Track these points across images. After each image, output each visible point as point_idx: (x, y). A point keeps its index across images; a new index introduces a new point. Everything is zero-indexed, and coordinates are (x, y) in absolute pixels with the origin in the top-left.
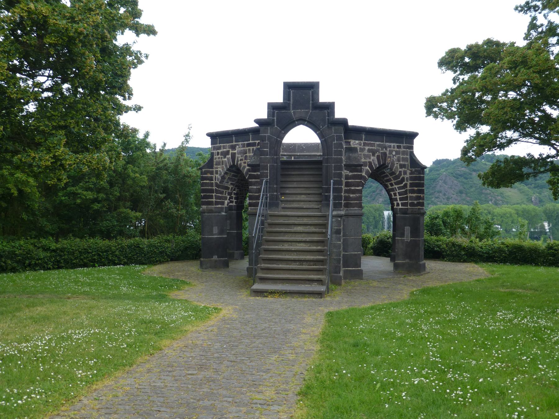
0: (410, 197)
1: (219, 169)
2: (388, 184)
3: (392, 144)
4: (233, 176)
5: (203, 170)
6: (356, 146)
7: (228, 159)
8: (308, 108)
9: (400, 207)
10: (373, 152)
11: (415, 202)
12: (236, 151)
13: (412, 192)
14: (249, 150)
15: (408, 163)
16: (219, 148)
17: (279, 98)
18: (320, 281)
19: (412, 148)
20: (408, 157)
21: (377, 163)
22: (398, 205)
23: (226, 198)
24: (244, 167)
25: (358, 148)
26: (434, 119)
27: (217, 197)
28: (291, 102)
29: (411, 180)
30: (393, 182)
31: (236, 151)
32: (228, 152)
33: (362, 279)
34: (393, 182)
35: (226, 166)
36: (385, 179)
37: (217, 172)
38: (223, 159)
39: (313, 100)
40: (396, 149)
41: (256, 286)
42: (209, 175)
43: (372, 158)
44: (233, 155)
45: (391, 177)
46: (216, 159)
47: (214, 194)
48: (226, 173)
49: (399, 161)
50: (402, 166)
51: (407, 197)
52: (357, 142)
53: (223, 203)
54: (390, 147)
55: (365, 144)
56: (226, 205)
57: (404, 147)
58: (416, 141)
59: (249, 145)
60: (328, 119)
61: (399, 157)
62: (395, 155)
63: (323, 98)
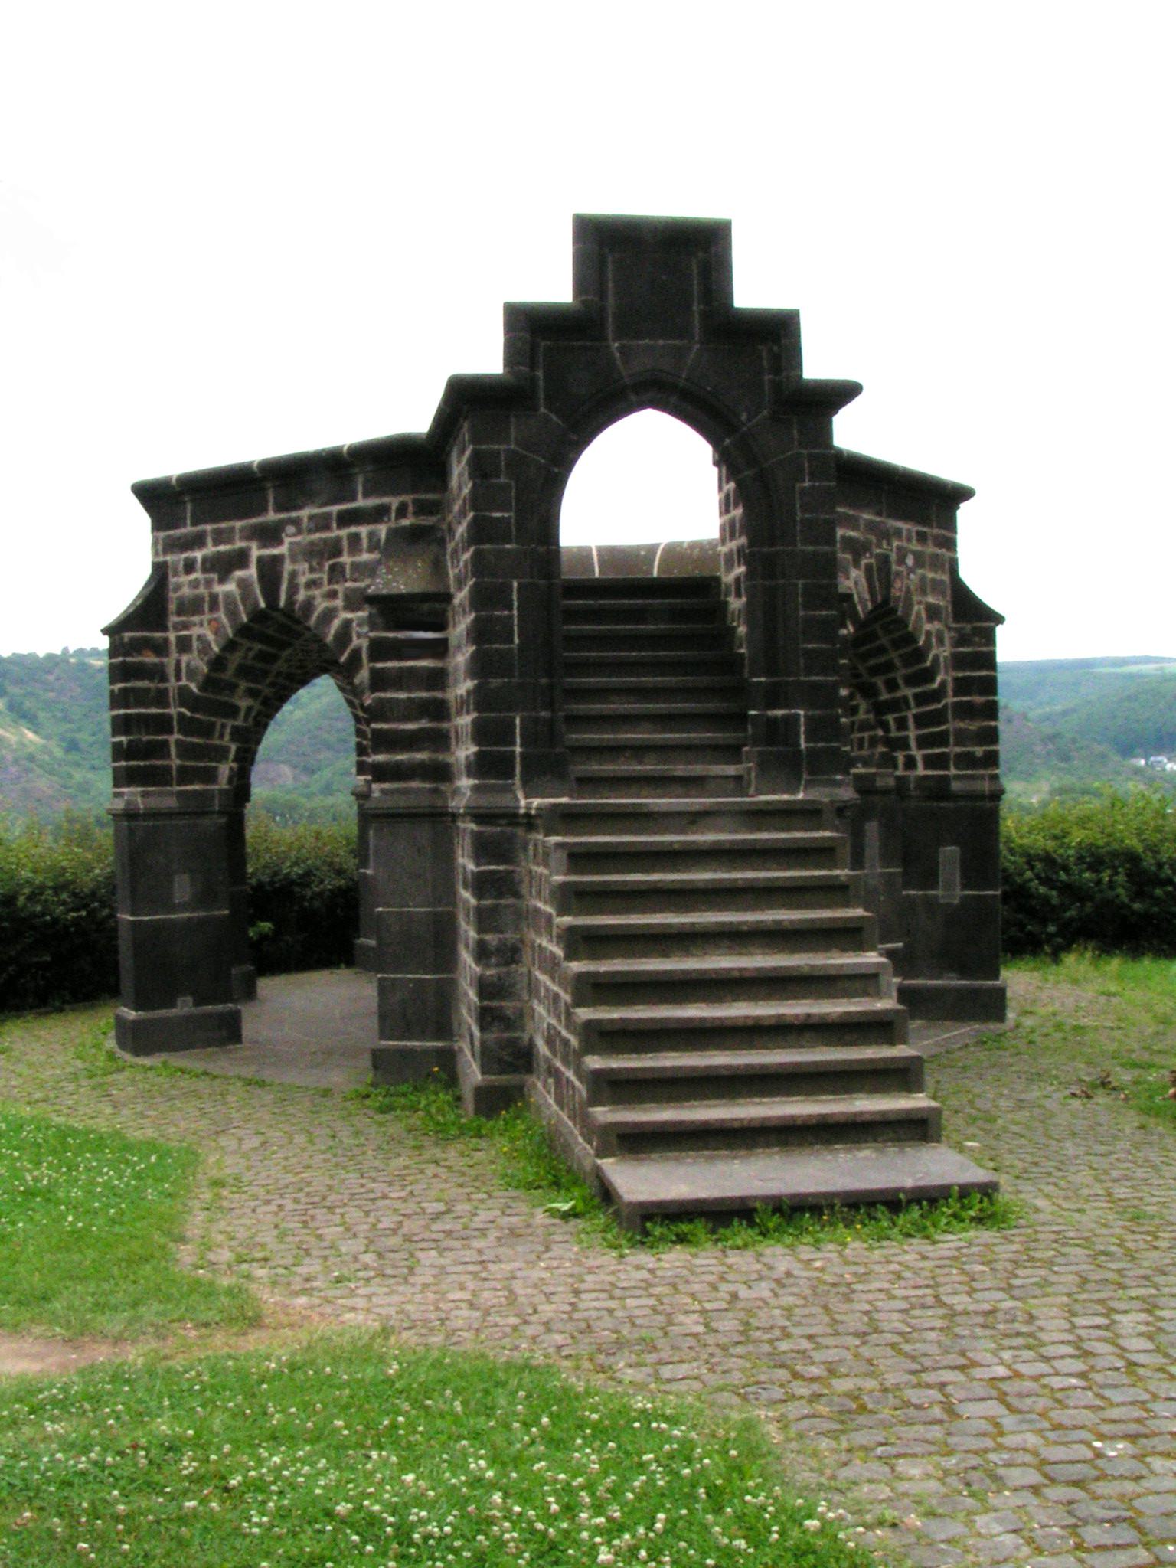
1: (195, 632)
2: (879, 681)
4: (262, 657)
5: (127, 635)
7: (243, 584)
8: (684, 332)
9: (921, 771)
12: (283, 550)
14: (355, 539)
15: (943, 602)
16: (198, 541)
17: (555, 286)
19: (950, 544)
20: (946, 578)
21: (867, 596)
23: (221, 754)
27: (185, 750)
28: (611, 302)
31: (283, 550)
34: (899, 674)
35: (232, 614)
37: (184, 645)
38: (220, 589)
40: (915, 546)
42: (150, 659)
44: (270, 570)
45: (894, 655)
48: (230, 646)
50: (933, 613)
53: (210, 776)
54: (898, 533)
58: (965, 513)
59: (346, 519)
63: (750, 292)
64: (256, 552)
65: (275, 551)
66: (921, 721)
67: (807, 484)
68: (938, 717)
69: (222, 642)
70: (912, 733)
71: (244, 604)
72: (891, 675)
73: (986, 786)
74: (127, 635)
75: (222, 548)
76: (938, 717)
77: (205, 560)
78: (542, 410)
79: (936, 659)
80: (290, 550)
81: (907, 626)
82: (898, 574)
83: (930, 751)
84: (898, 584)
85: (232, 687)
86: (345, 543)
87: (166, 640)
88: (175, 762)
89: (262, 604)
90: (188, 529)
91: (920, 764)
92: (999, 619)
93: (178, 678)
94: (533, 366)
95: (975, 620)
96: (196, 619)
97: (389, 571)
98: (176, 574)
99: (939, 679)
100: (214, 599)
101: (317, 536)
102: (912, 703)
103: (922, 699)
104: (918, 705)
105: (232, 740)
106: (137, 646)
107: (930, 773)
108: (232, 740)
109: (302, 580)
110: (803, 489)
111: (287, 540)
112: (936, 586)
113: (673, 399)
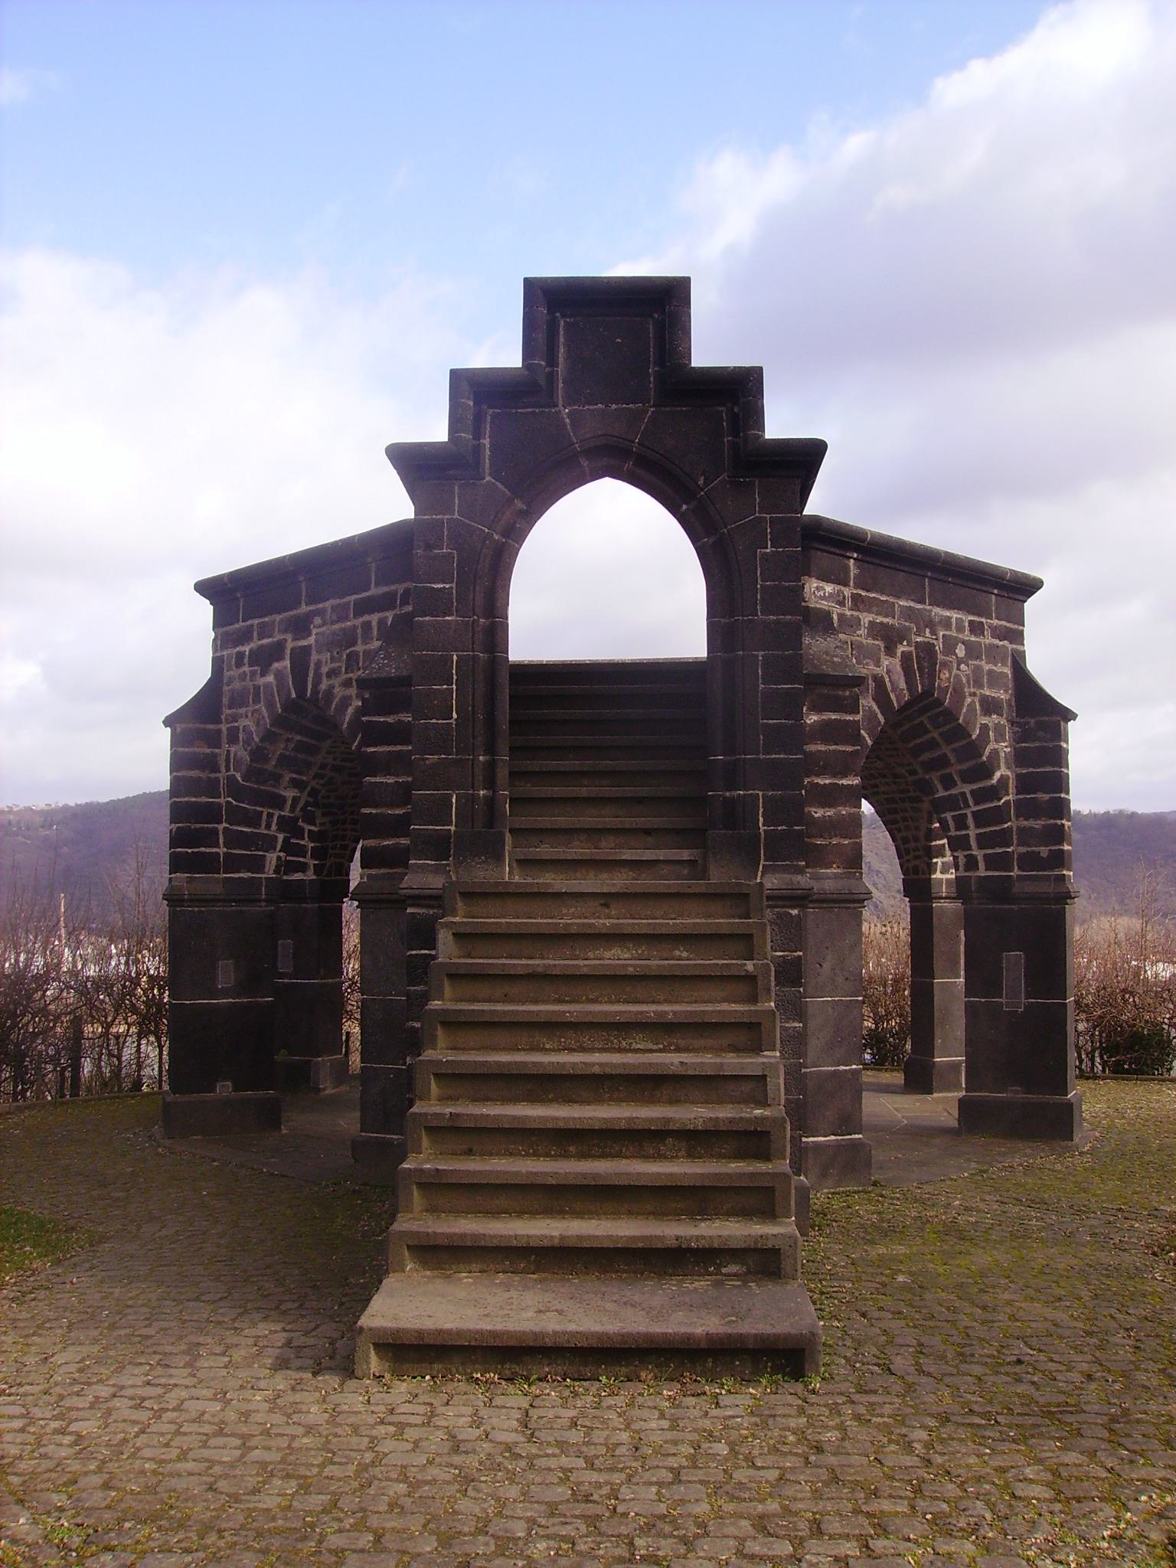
0: (1022, 830)
1: (242, 723)
2: (935, 777)
3: (954, 615)
4: (301, 747)
6: (824, 605)
7: (279, 675)
9: (982, 872)
12: (312, 640)
14: (367, 626)
16: (245, 637)
17: (502, 349)
19: (1017, 637)
20: (1008, 671)
21: (903, 685)
23: (269, 843)
24: (345, 702)
25: (835, 617)
27: (233, 839)
32: (280, 646)
34: (955, 769)
35: (270, 705)
36: (925, 757)
37: (233, 738)
38: (261, 681)
39: (661, 362)
40: (967, 636)
44: (301, 659)
45: (946, 749)
46: (231, 680)
47: (221, 827)
48: (269, 737)
50: (990, 706)
52: (829, 588)
53: (258, 864)
54: (946, 623)
55: (858, 602)
56: (269, 872)
59: (365, 607)
61: (978, 668)
63: (710, 347)
65: (304, 643)
66: (980, 819)
70: (972, 832)
72: (947, 771)
73: (1050, 888)
75: (265, 641)
78: (488, 478)
79: (995, 752)
82: (944, 664)
83: (990, 851)
84: (945, 675)
85: (277, 778)
87: (219, 731)
89: (294, 695)
91: (982, 865)
92: (1068, 715)
93: (228, 769)
94: (478, 435)
95: (1041, 719)
96: (242, 711)
99: (997, 775)
101: (336, 627)
103: (981, 796)
105: (280, 829)
107: (990, 873)
108: (280, 829)
111: (314, 631)
112: (994, 679)
113: (629, 464)
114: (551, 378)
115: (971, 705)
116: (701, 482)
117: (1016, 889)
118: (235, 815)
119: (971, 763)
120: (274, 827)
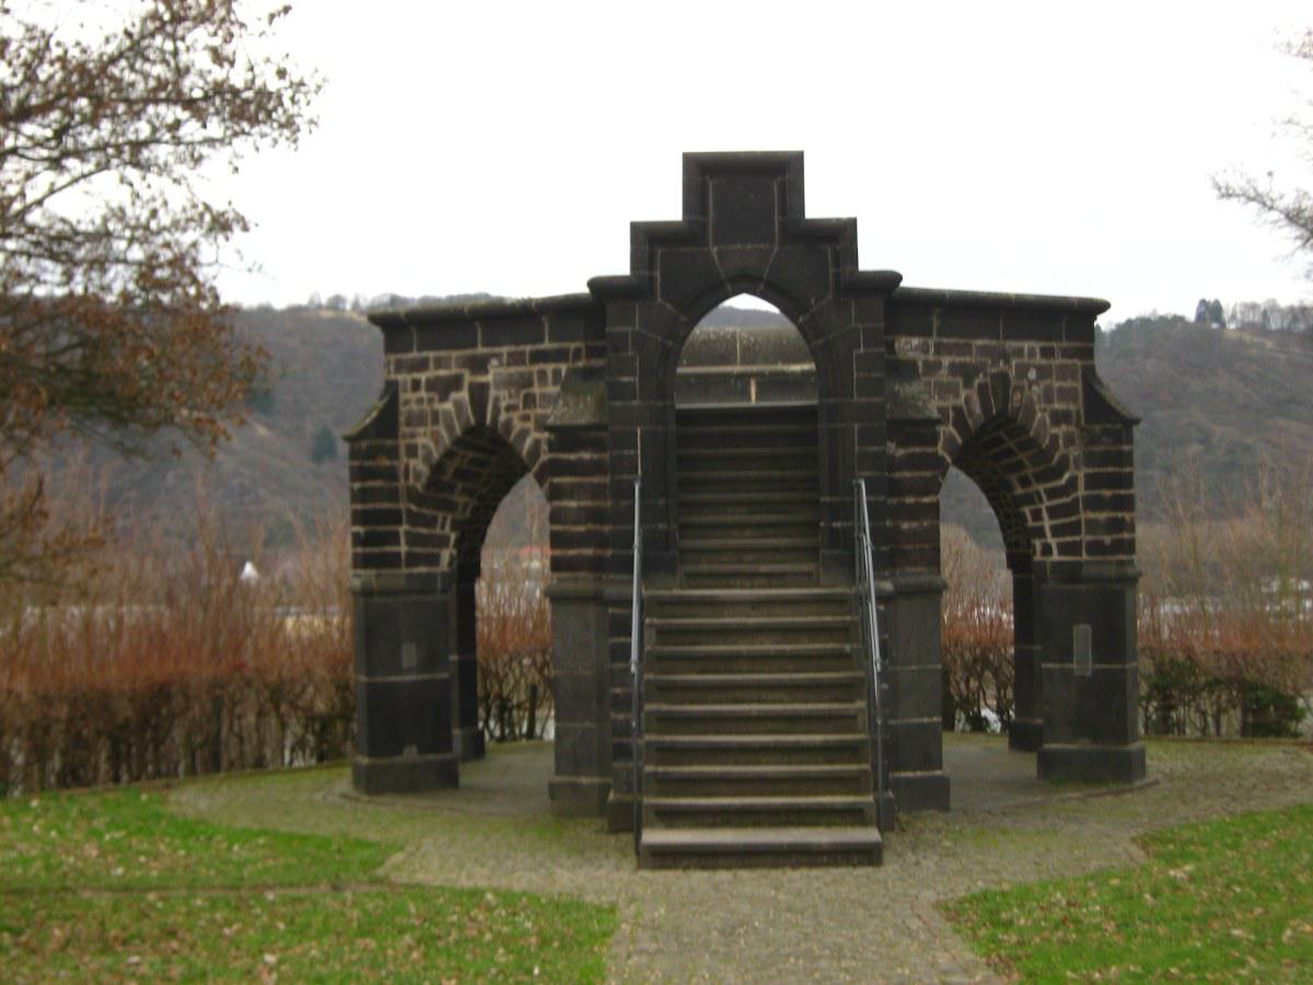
0: (1089, 522)
2: (1014, 478)
3: (1026, 345)
5: (364, 444)
6: (911, 355)
7: (458, 404)
9: (1056, 557)
10: (966, 373)
11: (1107, 539)
12: (489, 378)
13: (1095, 504)
14: (542, 374)
16: (422, 365)
17: (668, 207)
18: (853, 816)
20: (1079, 385)
21: (978, 410)
22: (1047, 550)
23: (443, 542)
25: (920, 363)
26: (1210, 298)
27: (413, 540)
29: (1087, 465)
30: (1029, 471)
31: (489, 378)
33: (946, 808)
34: (1029, 471)
35: (450, 428)
36: (1004, 462)
38: (438, 406)
39: (783, 212)
40: (1039, 360)
41: (654, 836)
42: (386, 462)
43: (963, 394)
44: (479, 394)
45: (1022, 456)
48: (449, 455)
49: (1048, 398)
50: (1059, 418)
51: (1079, 522)
52: (915, 341)
53: (434, 560)
54: (1019, 352)
55: (939, 349)
57: (1066, 353)
59: (538, 357)
60: (837, 276)
62: (1036, 382)
63: (819, 205)
64: (468, 378)
67: (862, 350)
68: (1072, 509)
69: (441, 450)
71: (459, 420)
74: (364, 444)
76: (1072, 509)
77: (428, 381)
78: (659, 300)
80: (495, 380)
81: (1027, 433)
86: (535, 377)
88: (403, 548)
90: (414, 355)
91: (1055, 551)
97: (566, 404)
98: (405, 391)
100: (435, 415)
102: (1044, 497)
104: (1050, 498)
106: (371, 454)
108: (453, 528)
109: (503, 404)
110: (859, 356)
114: (704, 226)
115: (1043, 419)
116: (813, 301)
117: (1085, 571)
118: (415, 519)
119: (1043, 467)
120: (448, 527)
